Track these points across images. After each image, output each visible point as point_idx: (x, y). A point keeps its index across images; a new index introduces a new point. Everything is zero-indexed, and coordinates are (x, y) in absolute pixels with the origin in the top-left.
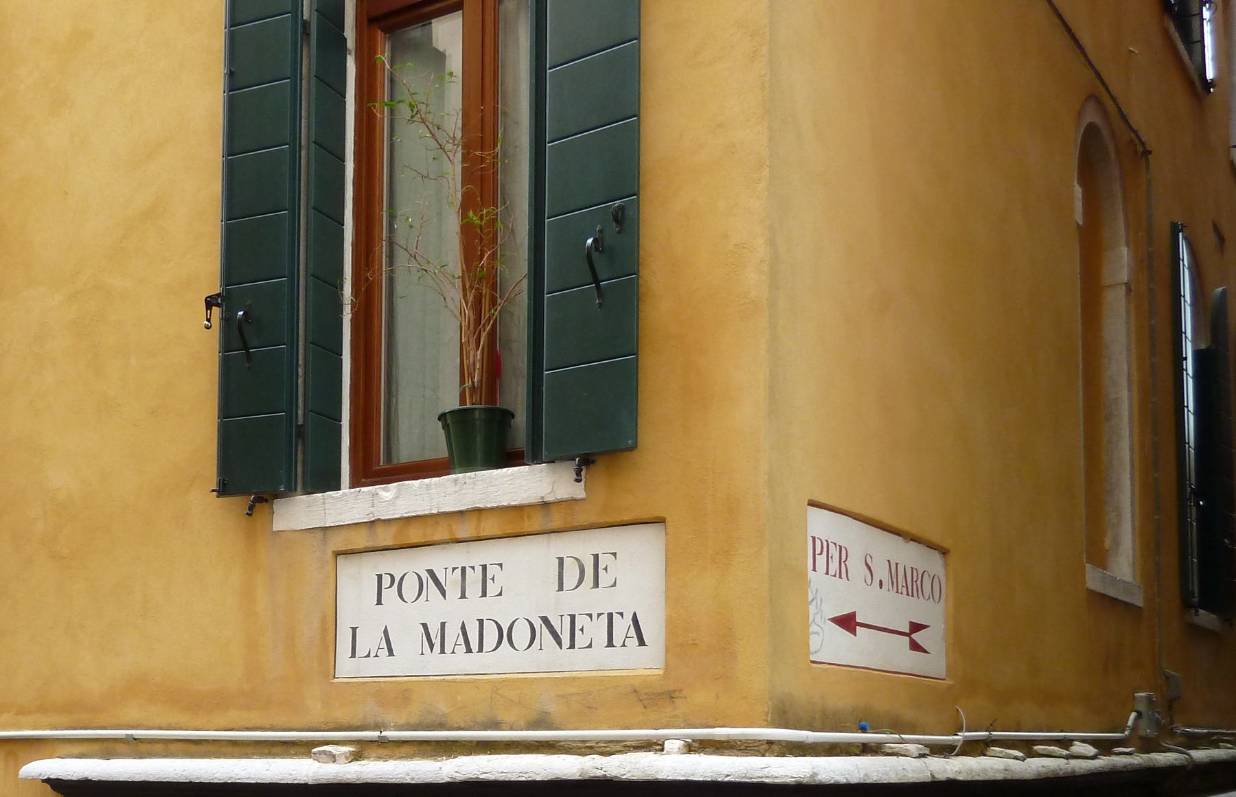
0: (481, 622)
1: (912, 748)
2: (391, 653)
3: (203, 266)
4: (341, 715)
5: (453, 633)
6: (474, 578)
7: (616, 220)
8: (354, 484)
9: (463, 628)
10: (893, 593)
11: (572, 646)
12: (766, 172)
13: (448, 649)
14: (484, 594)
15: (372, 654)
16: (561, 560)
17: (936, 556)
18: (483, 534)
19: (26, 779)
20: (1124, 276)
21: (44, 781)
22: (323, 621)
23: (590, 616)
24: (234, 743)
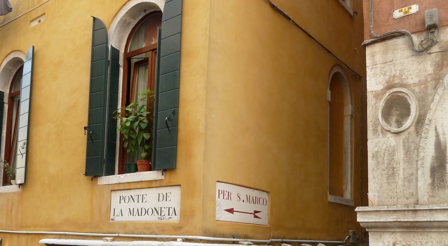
0: (142, 208)
1: (246, 243)
2: (122, 215)
3: (84, 121)
4: (110, 230)
5: (136, 211)
6: (141, 197)
7: (173, 113)
8: (119, 174)
10: (248, 203)
12: (205, 102)
16: (159, 194)
17: (265, 193)
18: (143, 187)
19: (40, 243)
20: (350, 114)
21: (45, 244)
22: (108, 207)
24: (87, 236)
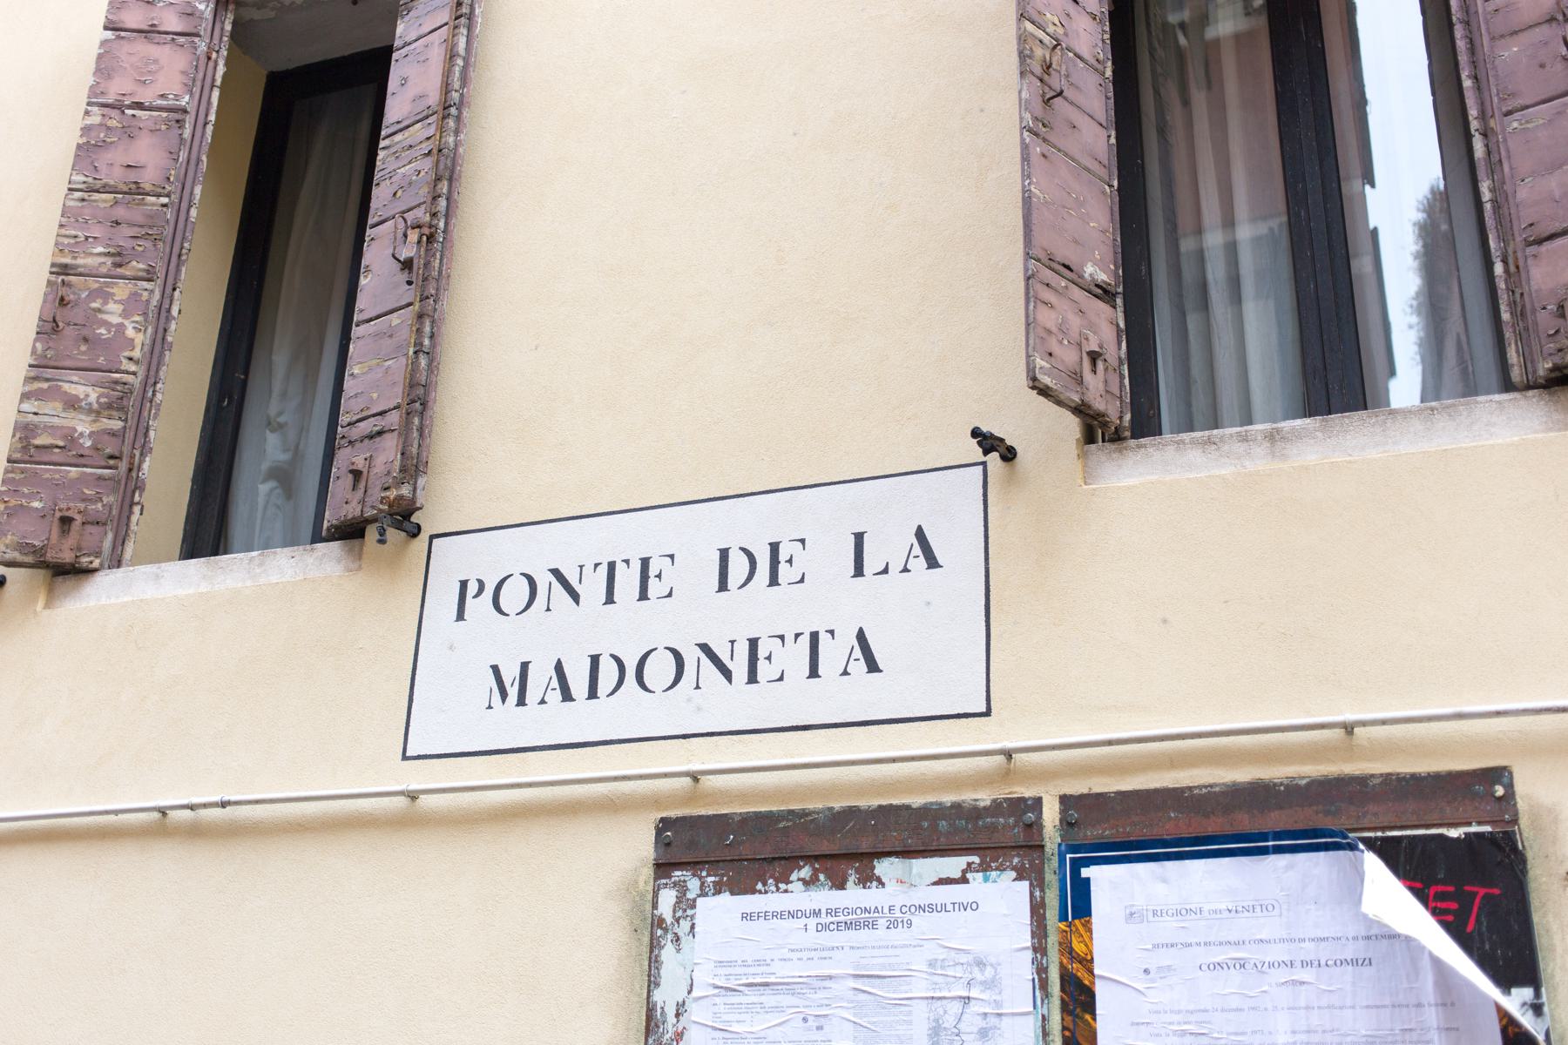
5: (541, 676)
9: (559, 668)
11: (752, 678)
13: (532, 695)
14: (643, 596)
15: (895, 568)
23: (782, 637)
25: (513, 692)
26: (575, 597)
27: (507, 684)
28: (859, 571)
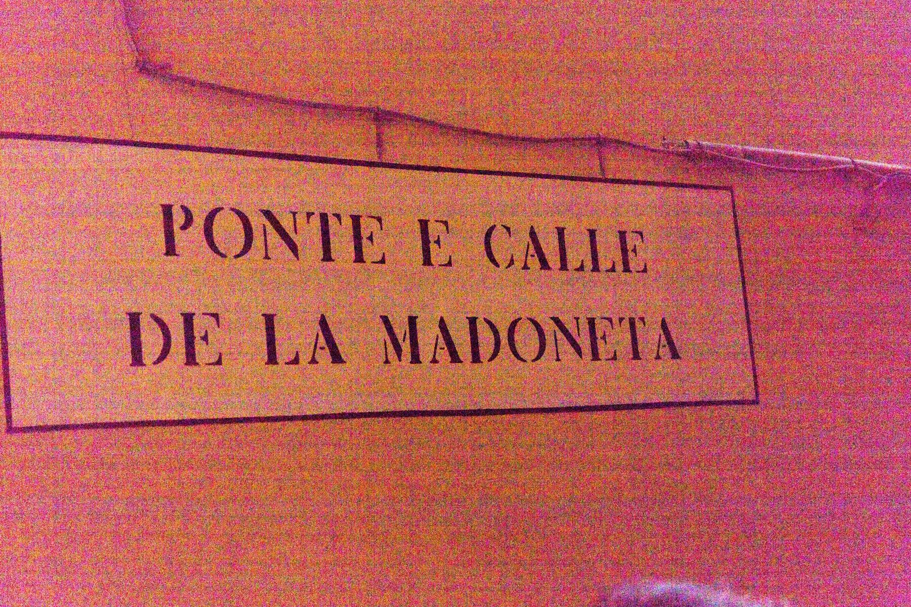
13: (426, 352)
15: (304, 359)
25: (406, 347)
26: (293, 247)
27: (400, 337)
28: (272, 358)
